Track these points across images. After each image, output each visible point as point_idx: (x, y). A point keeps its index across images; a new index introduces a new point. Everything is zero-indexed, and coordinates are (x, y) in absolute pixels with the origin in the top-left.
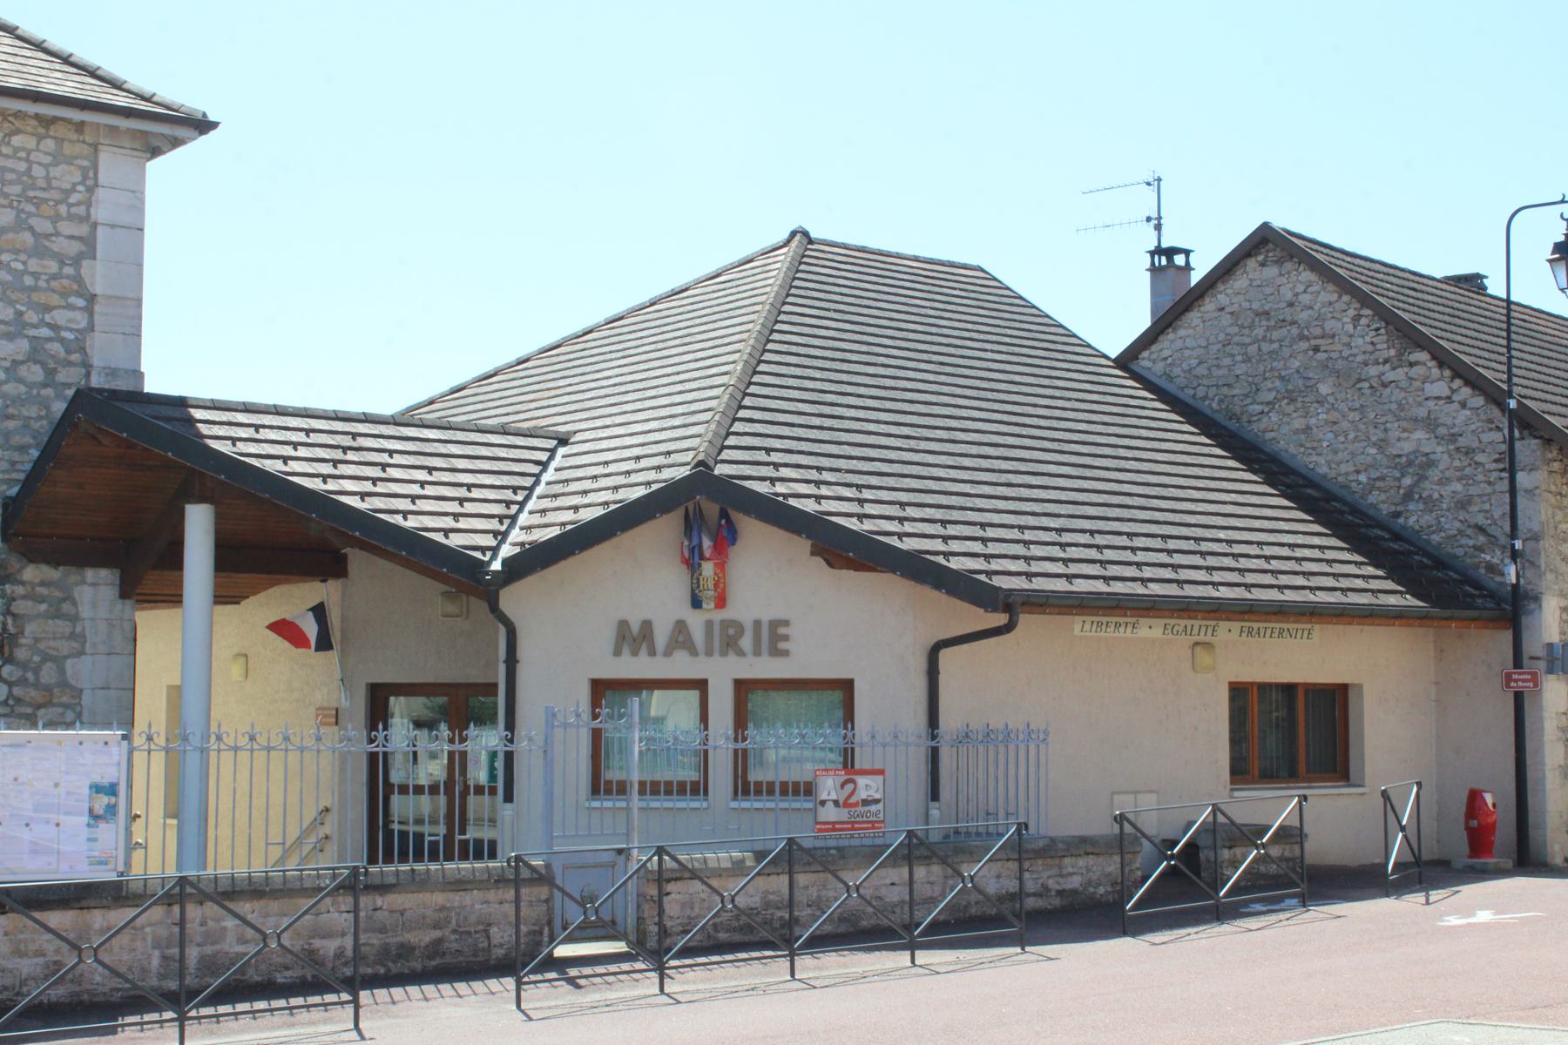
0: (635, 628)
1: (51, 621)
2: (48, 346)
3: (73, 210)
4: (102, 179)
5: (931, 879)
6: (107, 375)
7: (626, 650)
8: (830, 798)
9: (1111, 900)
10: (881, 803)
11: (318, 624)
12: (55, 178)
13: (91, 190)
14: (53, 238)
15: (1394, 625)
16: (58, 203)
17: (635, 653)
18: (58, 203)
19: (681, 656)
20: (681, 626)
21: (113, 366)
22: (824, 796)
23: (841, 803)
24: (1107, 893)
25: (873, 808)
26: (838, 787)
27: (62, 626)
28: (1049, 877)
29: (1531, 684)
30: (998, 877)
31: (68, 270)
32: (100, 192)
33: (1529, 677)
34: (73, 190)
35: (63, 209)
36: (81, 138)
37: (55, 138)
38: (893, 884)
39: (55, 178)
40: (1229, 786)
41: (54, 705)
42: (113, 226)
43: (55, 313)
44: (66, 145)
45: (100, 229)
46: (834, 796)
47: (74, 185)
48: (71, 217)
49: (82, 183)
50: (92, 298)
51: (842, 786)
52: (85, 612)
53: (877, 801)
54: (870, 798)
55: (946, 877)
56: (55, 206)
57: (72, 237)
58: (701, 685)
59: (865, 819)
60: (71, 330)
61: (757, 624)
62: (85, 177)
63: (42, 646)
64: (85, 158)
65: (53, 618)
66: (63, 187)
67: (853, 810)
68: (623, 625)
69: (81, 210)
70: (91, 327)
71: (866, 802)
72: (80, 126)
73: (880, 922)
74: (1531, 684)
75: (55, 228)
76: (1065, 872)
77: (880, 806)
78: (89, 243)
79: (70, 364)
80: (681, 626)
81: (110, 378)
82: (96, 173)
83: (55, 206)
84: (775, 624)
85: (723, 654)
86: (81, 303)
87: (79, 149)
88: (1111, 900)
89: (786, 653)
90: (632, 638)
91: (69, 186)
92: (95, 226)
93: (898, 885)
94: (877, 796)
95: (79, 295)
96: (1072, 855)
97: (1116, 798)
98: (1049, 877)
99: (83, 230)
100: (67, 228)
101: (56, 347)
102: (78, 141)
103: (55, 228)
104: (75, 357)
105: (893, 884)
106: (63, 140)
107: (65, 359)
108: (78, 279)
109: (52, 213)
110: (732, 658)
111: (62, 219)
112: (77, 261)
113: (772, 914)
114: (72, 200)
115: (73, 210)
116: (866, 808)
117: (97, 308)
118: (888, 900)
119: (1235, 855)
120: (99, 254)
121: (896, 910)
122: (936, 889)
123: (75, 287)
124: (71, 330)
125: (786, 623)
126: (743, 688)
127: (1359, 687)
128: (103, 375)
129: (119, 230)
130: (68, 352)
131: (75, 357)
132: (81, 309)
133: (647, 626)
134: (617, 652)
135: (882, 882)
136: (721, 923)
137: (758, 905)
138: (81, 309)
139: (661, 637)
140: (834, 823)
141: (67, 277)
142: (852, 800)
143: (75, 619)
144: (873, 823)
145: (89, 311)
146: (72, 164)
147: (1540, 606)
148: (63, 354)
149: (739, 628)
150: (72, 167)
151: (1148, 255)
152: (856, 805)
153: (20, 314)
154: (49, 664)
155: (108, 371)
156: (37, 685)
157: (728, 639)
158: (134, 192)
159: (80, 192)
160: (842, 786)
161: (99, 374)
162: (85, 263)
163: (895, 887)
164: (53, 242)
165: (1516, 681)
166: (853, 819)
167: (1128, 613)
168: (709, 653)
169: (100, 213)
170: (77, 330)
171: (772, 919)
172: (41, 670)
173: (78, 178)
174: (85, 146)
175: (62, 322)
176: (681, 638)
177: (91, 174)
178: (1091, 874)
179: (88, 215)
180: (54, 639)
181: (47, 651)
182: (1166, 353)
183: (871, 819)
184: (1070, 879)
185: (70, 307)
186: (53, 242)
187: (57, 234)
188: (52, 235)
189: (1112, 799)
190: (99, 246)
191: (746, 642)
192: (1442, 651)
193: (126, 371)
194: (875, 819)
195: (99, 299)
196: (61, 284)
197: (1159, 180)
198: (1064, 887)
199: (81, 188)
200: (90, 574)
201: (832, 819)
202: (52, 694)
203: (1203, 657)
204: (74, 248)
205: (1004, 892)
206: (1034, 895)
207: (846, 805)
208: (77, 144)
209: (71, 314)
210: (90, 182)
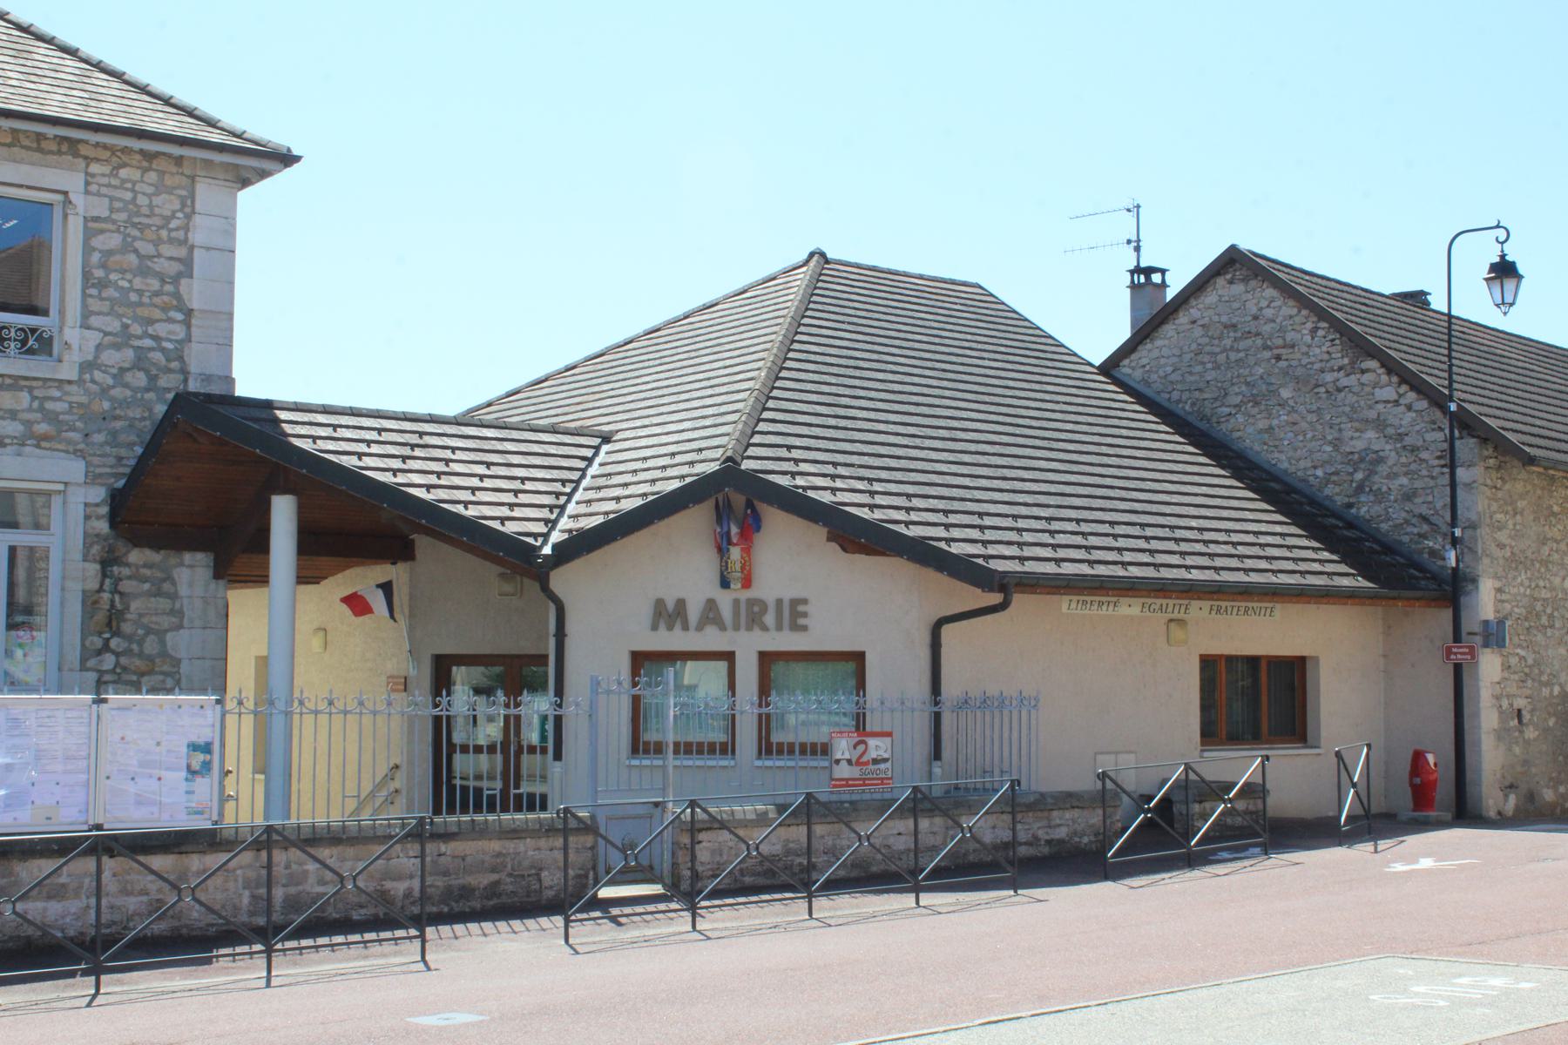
0: (670, 605)
1: (153, 599)
2: (151, 355)
3: (174, 234)
4: (198, 207)
5: (935, 829)
6: (203, 380)
7: (662, 626)
12: (158, 206)
13: (189, 217)
14: (156, 260)
16: (160, 228)
17: (670, 628)
18: (160, 228)
19: (711, 631)
20: (711, 604)
23: (854, 760)
24: (1090, 842)
25: (882, 766)
27: (164, 603)
28: (1039, 828)
30: (994, 827)
31: (169, 288)
32: (197, 219)
33: (1467, 650)
34: (173, 216)
35: (164, 233)
36: (180, 171)
38: (899, 834)
39: (158, 206)
40: (1200, 748)
41: (157, 673)
42: (208, 249)
43: (157, 326)
44: (167, 177)
45: (197, 252)
46: (847, 756)
47: (174, 212)
48: (171, 241)
49: (181, 210)
50: (189, 313)
52: (183, 590)
55: (947, 828)
57: (171, 258)
58: (729, 657)
62: (184, 205)
63: (145, 620)
68: (659, 604)
69: (180, 234)
70: (189, 339)
71: (875, 761)
72: (179, 161)
75: (157, 250)
76: (1053, 823)
77: (888, 765)
78: (187, 263)
79: (170, 371)
80: (711, 604)
82: (193, 202)
84: (795, 603)
85: (749, 628)
86: (180, 316)
87: (178, 180)
89: (804, 628)
90: (669, 614)
91: (169, 214)
92: (192, 248)
94: (886, 756)
95: (178, 309)
96: (1060, 809)
97: (1100, 757)
98: (1039, 828)
99: (182, 252)
102: (178, 173)
103: (157, 250)
104: (175, 365)
105: (899, 834)
107: (166, 366)
108: (177, 295)
109: (154, 237)
112: (176, 280)
114: (173, 225)
115: (174, 234)
116: (876, 767)
119: (1204, 808)
123: (175, 303)
124: (170, 341)
125: (805, 601)
126: (767, 659)
127: (1316, 659)
129: (213, 251)
130: (168, 360)
132: (179, 322)
133: (681, 604)
134: (655, 627)
138: (179, 322)
139: (694, 614)
140: (847, 780)
141: (168, 294)
142: (864, 759)
143: (174, 596)
145: (187, 323)
146: (173, 194)
147: (1477, 588)
149: (762, 604)
150: (172, 197)
152: (867, 763)
153: (126, 326)
156: (141, 655)
157: (753, 615)
158: (226, 218)
159: (178, 218)
161: (196, 380)
162: (184, 281)
168: (736, 628)
169: (197, 237)
170: (177, 341)
171: (792, 866)
173: (178, 207)
175: (163, 335)
176: (711, 615)
180: (156, 614)
184: (1058, 830)
185: (170, 320)
187: (159, 256)
188: (155, 257)
191: (770, 619)
195: (196, 313)
197: (1138, 207)
198: (1052, 836)
199: (180, 215)
200: (188, 557)
201: (846, 775)
204: (174, 268)
207: (858, 763)
209: (171, 327)
210: (188, 210)
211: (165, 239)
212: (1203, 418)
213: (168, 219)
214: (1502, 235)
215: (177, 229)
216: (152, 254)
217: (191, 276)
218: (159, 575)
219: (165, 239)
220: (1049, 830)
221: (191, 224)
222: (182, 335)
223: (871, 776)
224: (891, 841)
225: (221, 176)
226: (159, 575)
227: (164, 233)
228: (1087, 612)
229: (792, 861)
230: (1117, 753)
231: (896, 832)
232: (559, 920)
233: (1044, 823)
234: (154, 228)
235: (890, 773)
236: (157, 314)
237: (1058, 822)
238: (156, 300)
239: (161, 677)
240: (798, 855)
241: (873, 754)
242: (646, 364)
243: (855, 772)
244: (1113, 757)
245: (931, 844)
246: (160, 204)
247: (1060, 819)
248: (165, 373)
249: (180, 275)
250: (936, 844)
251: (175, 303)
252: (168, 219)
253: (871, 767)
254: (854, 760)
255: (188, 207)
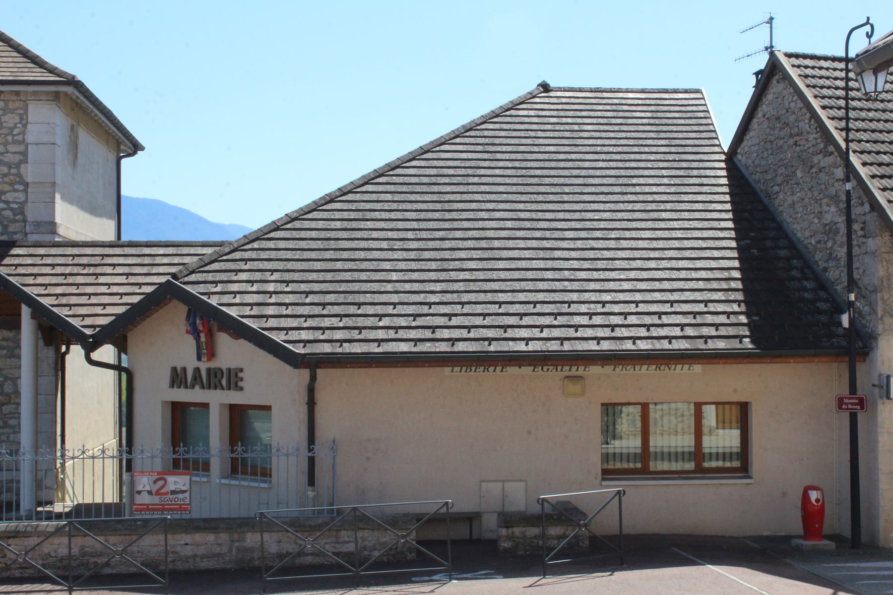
1: (8, 360)
2: (4, 213)
3: (16, 138)
4: (30, 120)
5: (220, 542)
6: (35, 225)
8: (144, 489)
9: (385, 560)
10: (188, 493)
11: (95, 361)
12: (5, 122)
13: (25, 126)
14: (6, 155)
15: (719, 363)
16: (6, 135)
18: (6, 135)
20: (197, 370)
21: (39, 220)
22: (140, 488)
23: (154, 492)
24: (382, 555)
25: (180, 496)
26: (151, 482)
28: (326, 543)
29: (859, 407)
30: (279, 542)
31: (14, 171)
32: (29, 126)
33: (857, 401)
34: (15, 127)
35: (10, 138)
36: (19, 98)
37: (4, 100)
38: (186, 544)
39: (5, 122)
40: (600, 476)
41: (12, 404)
42: (37, 144)
43: (8, 194)
44: (10, 103)
45: (30, 147)
46: (148, 488)
47: (16, 124)
48: (14, 142)
49: (20, 123)
50: (27, 185)
51: (155, 482)
53: (184, 492)
54: (177, 490)
55: (232, 541)
56: (5, 137)
57: (15, 153)
59: (173, 502)
60: (16, 203)
61: (229, 370)
62: (21, 119)
64: (21, 109)
65: (10, 357)
66: (10, 126)
67: (164, 497)
69: (20, 138)
70: (26, 201)
71: (173, 492)
72: (17, 93)
73: (176, 567)
74: (859, 407)
75: (6, 149)
76: (341, 540)
77: (187, 495)
78: (25, 154)
79: (16, 221)
80: (197, 370)
81: (36, 227)
82: (27, 116)
83: (5, 137)
85: (216, 388)
86: (21, 187)
87: (18, 104)
88: (385, 560)
89: (242, 389)
91: (12, 125)
92: (27, 144)
93: (191, 545)
94: (184, 488)
95: (20, 183)
96: (345, 530)
97: (483, 484)
98: (326, 543)
99: (21, 148)
100: (12, 148)
101: (7, 213)
102: (17, 100)
103: (6, 149)
104: (18, 217)
105: (186, 544)
106: (9, 100)
107: (13, 219)
108: (19, 175)
109: (4, 141)
110: (219, 392)
111: (10, 144)
112: (18, 166)
113: (89, 560)
114: (16, 132)
115: (16, 138)
116: (174, 496)
117: (29, 190)
118: (181, 554)
119: (513, 532)
120: (29, 160)
121: (189, 560)
122: (223, 548)
123: (18, 179)
124: (16, 203)
125: (241, 370)
127: (751, 402)
128: (32, 226)
129: (40, 146)
130: (15, 215)
131: (18, 217)
132: (21, 191)
135: (178, 543)
136: (49, 563)
137: (77, 554)
138: (21, 191)
140: (148, 505)
141: (14, 175)
142: (163, 491)
144: (180, 505)
145: (26, 191)
146: (14, 113)
147: (877, 344)
148: (12, 216)
150: (14, 115)
151: (754, 76)
152: (166, 493)
154: (9, 382)
155: (35, 223)
158: (49, 124)
159: (19, 128)
160: (155, 482)
161: (30, 225)
162: (22, 166)
163: (188, 546)
164: (6, 156)
165: (847, 404)
166: (163, 503)
167: (426, 365)
169: (30, 138)
170: (19, 203)
171: (88, 563)
172: (4, 385)
173: (18, 121)
174: (22, 103)
175: (11, 199)
177: (25, 117)
178: (366, 542)
179: (24, 139)
180: (11, 368)
181: (8, 375)
182: (746, 149)
183: (179, 502)
184: (346, 546)
185: (15, 191)
186: (6, 156)
187: (7, 152)
188: (5, 153)
189: (480, 486)
190: (29, 156)
192: (840, 376)
193: (46, 222)
194: (182, 502)
195: (30, 185)
196: (10, 179)
197: (772, 19)
198: (340, 550)
199: (19, 125)
201: (147, 502)
202: (10, 398)
203: (575, 388)
204: (18, 158)
205: (285, 552)
206: (312, 554)
207: (158, 493)
208: (17, 102)
209: (16, 194)
210: (24, 122)
211: (11, 141)
212: (768, 195)
213: (11, 129)
214: (868, 28)
215: (18, 134)
216: (2, 151)
217: (27, 163)
218: (12, 345)
219: (11, 141)
220: (336, 545)
221: (26, 130)
222: (23, 199)
223: (170, 503)
224: (178, 549)
225: (44, 98)
226: (12, 345)
227: (10, 138)
228: (472, 373)
229: (89, 560)
230: (504, 481)
231: (182, 542)
232: (626, 531)
233: (334, 539)
234: (3, 136)
235: (188, 501)
236: (7, 188)
237: (346, 539)
238: (6, 179)
239: (14, 406)
240: (93, 556)
241: (172, 487)
242: (562, 164)
243: (156, 500)
244: (500, 485)
245: (217, 552)
246: (7, 120)
247: (348, 537)
248: (13, 223)
249: (21, 162)
250: (222, 552)
251: (18, 179)
252: (11, 129)
253: (170, 496)
254: (154, 492)
255: (24, 121)
